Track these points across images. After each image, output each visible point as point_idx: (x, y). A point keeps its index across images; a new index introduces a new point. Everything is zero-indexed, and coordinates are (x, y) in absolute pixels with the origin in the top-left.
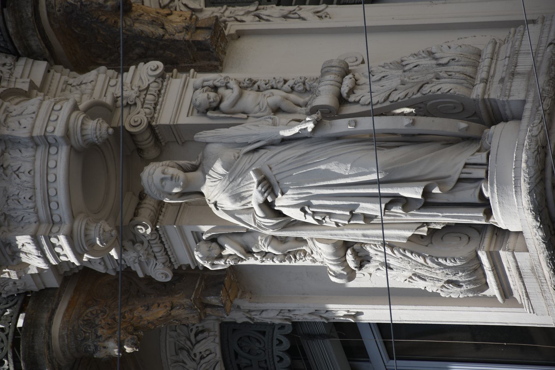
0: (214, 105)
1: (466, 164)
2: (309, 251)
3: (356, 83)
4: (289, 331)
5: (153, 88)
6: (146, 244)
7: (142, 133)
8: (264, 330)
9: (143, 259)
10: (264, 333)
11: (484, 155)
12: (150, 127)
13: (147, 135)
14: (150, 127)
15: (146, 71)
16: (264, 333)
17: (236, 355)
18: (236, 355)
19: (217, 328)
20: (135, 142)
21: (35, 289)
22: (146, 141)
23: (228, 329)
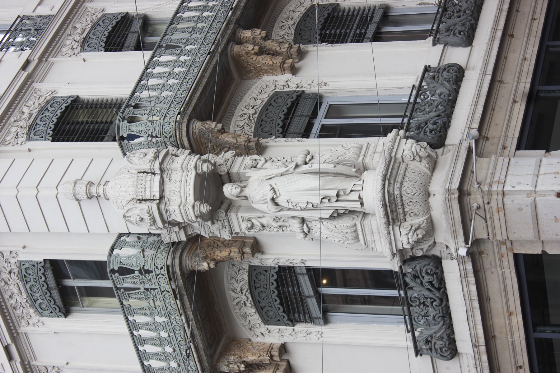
0: (254, 165)
1: (354, 185)
2: (288, 225)
3: (312, 158)
4: (277, 270)
5: (231, 160)
6: (222, 221)
7: (224, 175)
8: (266, 269)
9: (220, 228)
10: (266, 271)
11: (362, 181)
12: (228, 173)
13: (226, 176)
14: (228, 173)
15: (230, 154)
16: (266, 271)
17: (255, 281)
18: (255, 281)
19: (247, 268)
20: (221, 179)
21: (177, 241)
22: (225, 178)
23: (252, 269)
